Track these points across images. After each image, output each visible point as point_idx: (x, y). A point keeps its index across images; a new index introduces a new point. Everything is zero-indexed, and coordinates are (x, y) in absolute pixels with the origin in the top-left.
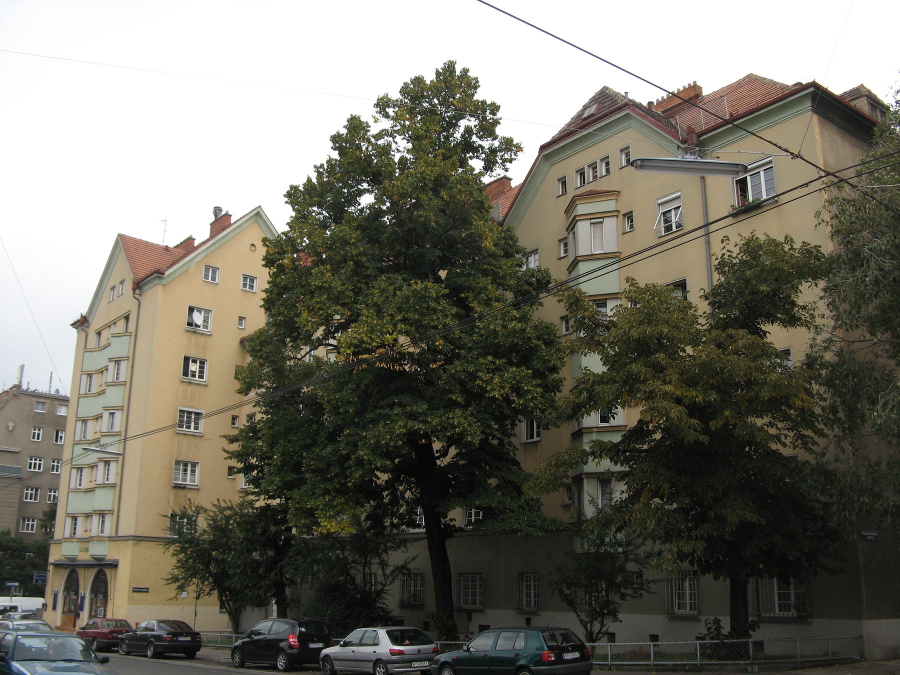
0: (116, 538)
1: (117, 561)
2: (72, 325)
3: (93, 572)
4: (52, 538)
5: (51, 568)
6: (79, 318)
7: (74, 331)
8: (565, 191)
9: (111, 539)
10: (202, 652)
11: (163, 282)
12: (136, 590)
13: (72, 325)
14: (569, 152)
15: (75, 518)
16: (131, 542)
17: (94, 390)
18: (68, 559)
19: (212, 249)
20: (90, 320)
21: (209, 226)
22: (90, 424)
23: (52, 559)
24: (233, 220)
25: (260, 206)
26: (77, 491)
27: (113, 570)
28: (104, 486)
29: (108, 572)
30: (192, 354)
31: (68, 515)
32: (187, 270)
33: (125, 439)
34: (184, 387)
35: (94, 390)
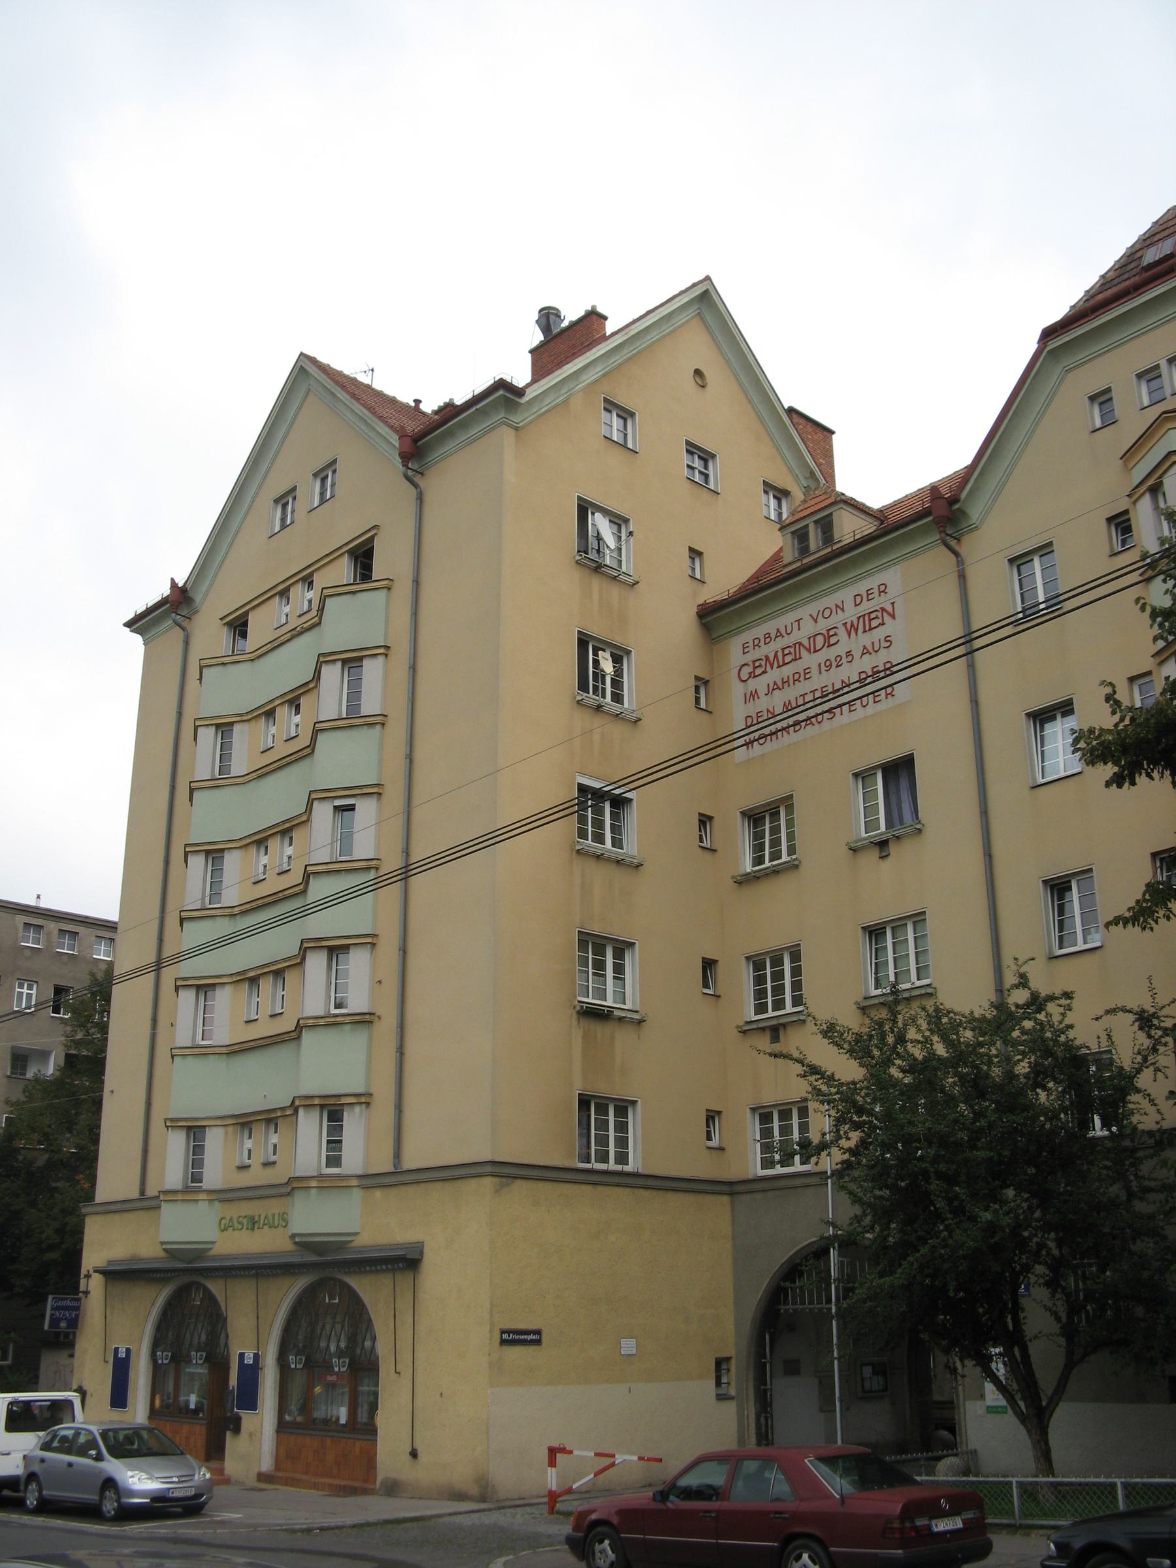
0: (396, 1178)
1: (419, 1248)
2: (128, 624)
3: (283, 1297)
4: (90, 1196)
5: (95, 1285)
6: (166, 591)
7: (136, 641)
8: (1109, 421)
9: (370, 1181)
10: (566, 1529)
11: (516, 418)
12: (514, 1338)
13: (128, 624)
14: (1082, 355)
15: (195, 1131)
16: (488, 1182)
17: (239, 767)
18: (171, 1253)
19: (618, 359)
20: (198, 598)
21: (528, 358)
22: (232, 862)
23: (93, 1257)
24: (610, 327)
25: (708, 279)
26: (198, 1052)
27: (409, 1276)
28: (329, 1023)
29: (371, 1291)
30: (594, 630)
31: (172, 1124)
32: (566, 402)
33: (158, 965)
34: (583, 719)
35: (239, 767)
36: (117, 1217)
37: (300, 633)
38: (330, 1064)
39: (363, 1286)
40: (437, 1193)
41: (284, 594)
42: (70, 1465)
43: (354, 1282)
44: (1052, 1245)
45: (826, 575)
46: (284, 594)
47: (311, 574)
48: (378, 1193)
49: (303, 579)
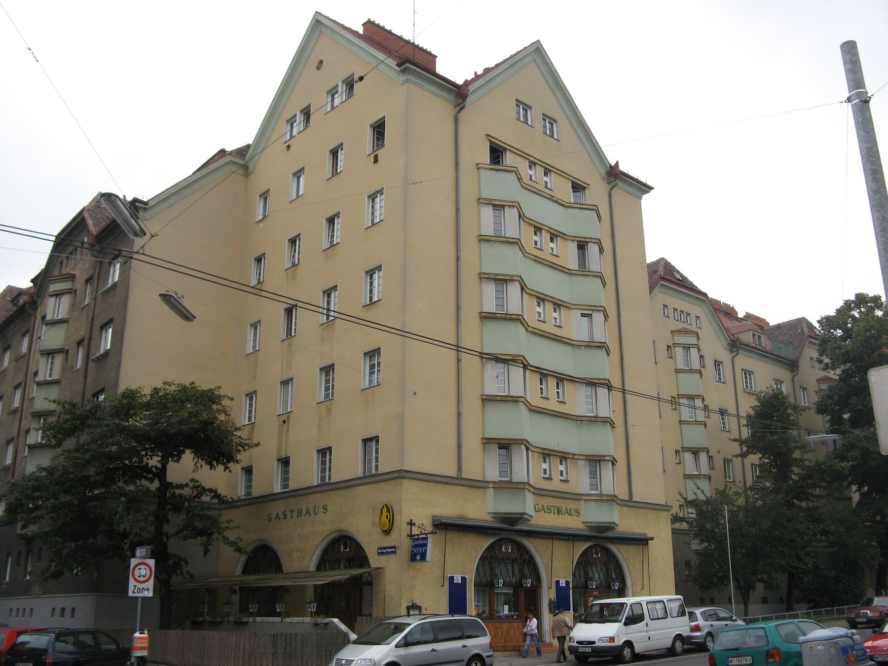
29: (624, 554)
36: (440, 486)
37: (554, 201)
38: (604, 442)
39: (620, 552)
40: (651, 514)
41: (532, 164)
42: (433, 650)
43: (613, 548)
44: (33, 528)
45: (749, 351)
46: (532, 164)
47: (550, 171)
48: (626, 509)
49: (530, 162)
